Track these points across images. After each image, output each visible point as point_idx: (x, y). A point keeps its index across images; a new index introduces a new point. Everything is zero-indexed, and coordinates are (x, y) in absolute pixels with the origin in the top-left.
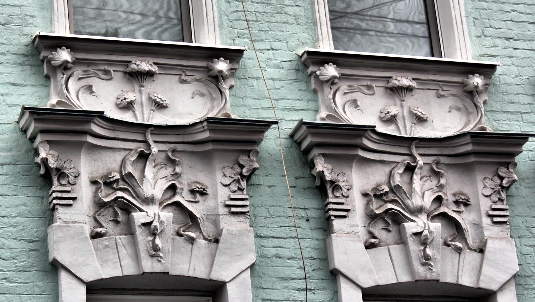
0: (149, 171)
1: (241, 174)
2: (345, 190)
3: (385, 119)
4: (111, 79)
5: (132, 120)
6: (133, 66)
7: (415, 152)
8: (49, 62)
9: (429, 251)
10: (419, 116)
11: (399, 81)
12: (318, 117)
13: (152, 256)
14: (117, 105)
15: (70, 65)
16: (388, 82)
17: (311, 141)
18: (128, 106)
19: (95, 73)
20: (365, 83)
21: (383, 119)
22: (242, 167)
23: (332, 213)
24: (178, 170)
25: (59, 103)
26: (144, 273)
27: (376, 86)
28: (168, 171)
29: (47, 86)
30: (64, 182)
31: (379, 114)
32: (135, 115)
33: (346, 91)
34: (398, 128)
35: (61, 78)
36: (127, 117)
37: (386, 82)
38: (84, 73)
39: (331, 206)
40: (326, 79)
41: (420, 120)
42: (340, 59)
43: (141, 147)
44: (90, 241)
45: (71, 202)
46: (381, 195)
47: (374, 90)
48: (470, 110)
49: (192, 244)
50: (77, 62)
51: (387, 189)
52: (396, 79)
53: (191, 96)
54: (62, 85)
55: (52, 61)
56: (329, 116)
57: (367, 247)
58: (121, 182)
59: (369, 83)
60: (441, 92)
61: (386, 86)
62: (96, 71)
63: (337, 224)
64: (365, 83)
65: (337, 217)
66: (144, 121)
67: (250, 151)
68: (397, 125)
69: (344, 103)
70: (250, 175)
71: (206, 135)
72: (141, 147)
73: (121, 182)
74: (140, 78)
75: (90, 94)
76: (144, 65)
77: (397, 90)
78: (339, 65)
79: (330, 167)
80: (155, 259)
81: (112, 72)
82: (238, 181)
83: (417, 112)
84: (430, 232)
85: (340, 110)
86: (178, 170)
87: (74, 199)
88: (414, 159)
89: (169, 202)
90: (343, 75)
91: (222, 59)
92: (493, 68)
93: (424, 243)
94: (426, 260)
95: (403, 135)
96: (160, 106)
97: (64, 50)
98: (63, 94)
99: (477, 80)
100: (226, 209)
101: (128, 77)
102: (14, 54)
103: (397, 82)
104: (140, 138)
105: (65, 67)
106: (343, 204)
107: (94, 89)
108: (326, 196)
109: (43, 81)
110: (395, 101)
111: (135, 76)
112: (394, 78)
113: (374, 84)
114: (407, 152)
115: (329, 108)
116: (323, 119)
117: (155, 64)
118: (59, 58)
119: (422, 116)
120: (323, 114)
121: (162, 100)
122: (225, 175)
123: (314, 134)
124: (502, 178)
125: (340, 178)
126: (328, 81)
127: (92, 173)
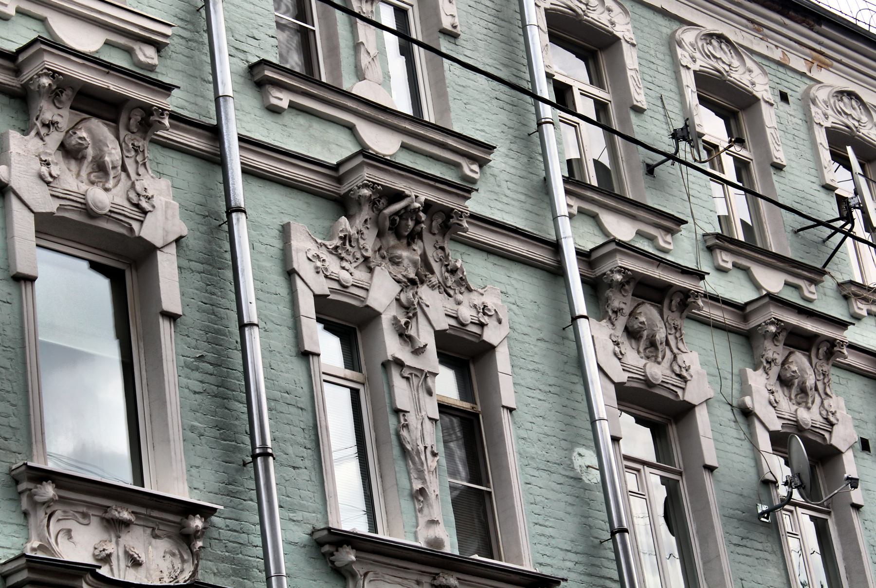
3: (100, 558)
8: (31, 497)
10: (136, 558)
11: (446, 579)
12: (29, 546)
16: (106, 512)
17: (27, 578)
19: (74, 515)
20: (81, 509)
21: (97, 557)
27: (92, 515)
29: (26, 526)
31: (92, 549)
32: (112, 570)
33: (61, 518)
34: (112, 570)
35: (42, 515)
37: (432, 578)
38: (63, 514)
40: (42, 501)
41: (136, 563)
42: (54, 476)
47: (90, 519)
48: (186, 557)
50: (62, 500)
52: (116, 510)
53: (162, 554)
54: (44, 526)
55: (35, 495)
56: (41, 548)
59: (85, 510)
60: (157, 531)
61: (104, 515)
62: (75, 514)
64: (81, 509)
66: (114, 576)
68: (111, 566)
69: (56, 532)
74: (117, 526)
75: (68, 539)
77: (114, 524)
78: (58, 487)
83: (133, 553)
85: (53, 541)
90: (60, 497)
91: (198, 515)
95: (116, 578)
96: (136, 563)
97: (49, 484)
98: (44, 537)
99: (197, 523)
101: (105, 523)
107: (73, 534)
109: (20, 520)
110: (110, 536)
111: (113, 524)
112: (114, 507)
113: (91, 512)
115: (41, 537)
116: (33, 550)
118: (44, 493)
119: (138, 559)
120: (36, 544)
121: (139, 557)
123: (31, 569)
126: (44, 503)
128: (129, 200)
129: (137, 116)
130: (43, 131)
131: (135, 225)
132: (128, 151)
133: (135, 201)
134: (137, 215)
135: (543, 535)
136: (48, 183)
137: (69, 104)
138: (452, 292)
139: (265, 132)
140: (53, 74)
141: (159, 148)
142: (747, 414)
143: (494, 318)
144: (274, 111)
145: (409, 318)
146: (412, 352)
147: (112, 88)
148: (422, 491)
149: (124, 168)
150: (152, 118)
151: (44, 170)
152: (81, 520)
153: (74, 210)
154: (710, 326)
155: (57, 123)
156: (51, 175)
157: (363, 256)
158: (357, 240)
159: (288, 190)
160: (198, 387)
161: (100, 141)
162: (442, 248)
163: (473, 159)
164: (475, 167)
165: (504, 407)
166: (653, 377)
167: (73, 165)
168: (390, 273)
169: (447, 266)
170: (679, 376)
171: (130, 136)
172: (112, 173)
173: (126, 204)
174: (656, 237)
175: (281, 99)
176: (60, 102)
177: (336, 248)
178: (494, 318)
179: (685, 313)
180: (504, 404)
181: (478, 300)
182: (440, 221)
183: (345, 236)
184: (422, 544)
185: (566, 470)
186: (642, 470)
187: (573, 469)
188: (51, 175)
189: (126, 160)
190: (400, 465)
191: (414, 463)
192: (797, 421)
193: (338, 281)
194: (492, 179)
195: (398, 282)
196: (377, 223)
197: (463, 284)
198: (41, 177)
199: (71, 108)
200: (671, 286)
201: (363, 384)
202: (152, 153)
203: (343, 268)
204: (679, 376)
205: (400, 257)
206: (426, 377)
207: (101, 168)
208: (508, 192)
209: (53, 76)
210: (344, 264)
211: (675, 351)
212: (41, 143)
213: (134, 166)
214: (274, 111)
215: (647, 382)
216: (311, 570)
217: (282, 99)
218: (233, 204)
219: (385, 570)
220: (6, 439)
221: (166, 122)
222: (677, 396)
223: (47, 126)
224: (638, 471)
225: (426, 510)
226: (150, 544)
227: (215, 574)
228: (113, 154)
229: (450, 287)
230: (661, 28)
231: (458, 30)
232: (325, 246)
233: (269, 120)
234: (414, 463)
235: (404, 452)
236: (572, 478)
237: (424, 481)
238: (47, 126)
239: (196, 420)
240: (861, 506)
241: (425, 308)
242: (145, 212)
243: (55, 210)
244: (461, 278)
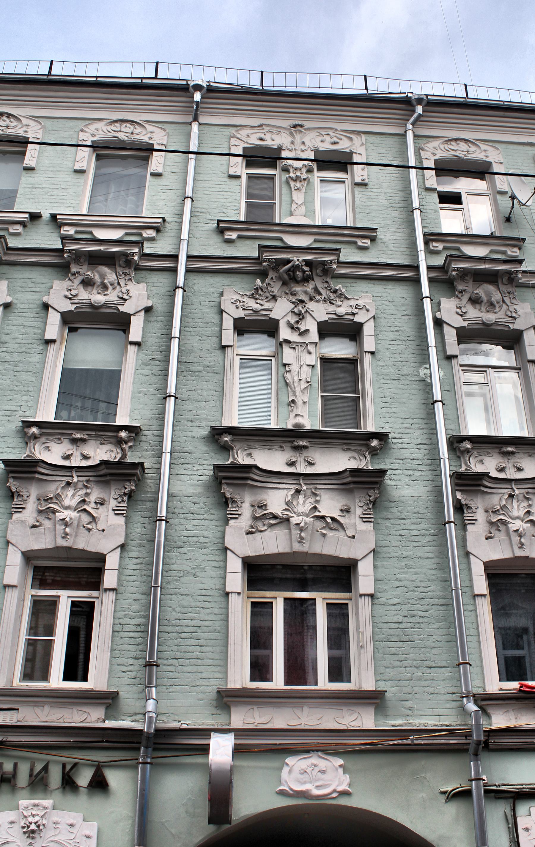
0: (515, 504)
1: (369, 500)
2: (239, 503)
4: (61, 443)
5: (295, 471)
6: (74, 436)
7: (514, 486)
8: (459, 449)
9: (523, 540)
13: (520, 548)
14: (287, 463)
15: (470, 450)
18: (502, 470)
22: (370, 496)
23: (466, 521)
24: (318, 498)
25: (466, 469)
26: (516, 557)
28: (525, 504)
30: (20, 499)
36: (502, 476)
39: (465, 518)
41: (86, 457)
43: (510, 491)
44: (245, 536)
45: (237, 516)
46: (262, 506)
49: (89, 532)
50: (43, 434)
51: (499, 508)
57: (487, 539)
58: (501, 510)
63: (469, 527)
65: (231, 518)
67: (131, 480)
70: (375, 501)
71: (349, 479)
72: (510, 491)
73: (501, 510)
76: (510, 449)
79: (465, 497)
80: (65, 540)
81: (284, 447)
82: (368, 504)
84: (524, 529)
86: (318, 498)
87: (476, 520)
88: (514, 491)
89: (80, 509)
92: (386, 435)
93: (520, 536)
94: (521, 546)
99: (375, 443)
100: (361, 520)
102: (158, 436)
103: (296, 443)
104: (509, 487)
105: (468, 451)
106: (473, 516)
108: (464, 512)
114: (70, 474)
117: (87, 434)
122: (116, 493)
124: (370, 496)
125: (237, 497)
127: (38, 495)
128: (118, 297)
129: (123, 259)
130: (460, 295)
131: (511, 326)
132: (120, 275)
133: (510, 315)
134: (122, 302)
135: (388, 413)
136: (461, 315)
137: (472, 279)
138: (334, 302)
139: (222, 252)
140: (458, 269)
141: (149, 272)
142: (221, 312)
143: (364, 309)
144: (229, 242)
145: (300, 319)
146: (299, 335)
147: (102, 249)
148: (293, 401)
149: (504, 302)
150: (512, 276)
151: (458, 310)
152: (57, 442)
153: (86, 307)
154: (530, 287)
155: (466, 290)
156: (71, 295)
157: (271, 295)
158: (267, 288)
159: (229, 275)
160: (149, 372)
161: (103, 274)
162: (327, 282)
163: (514, 246)
164: (516, 249)
165: (366, 352)
166: (487, 321)
167: (478, 306)
168: (288, 300)
169: (330, 290)
170: (511, 317)
171: (505, 286)
172: (497, 306)
173: (118, 299)
174: (506, 251)
175: (231, 235)
176: (467, 280)
177: (253, 295)
178: (364, 309)
179: (514, 284)
180: (365, 350)
181: (353, 303)
182: (507, 278)
183: (257, 288)
184: (290, 427)
185: (413, 377)
186: (488, 371)
187: (419, 376)
188: (71, 295)
189: (505, 298)
190: (284, 390)
191: (291, 388)
192: (91, 303)
193: (252, 310)
194: (382, 244)
195: (293, 303)
196: (280, 278)
197: (342, 297)
198: (66, 297)
199: (89, 264)
200: (498, 271)
201: (274, 356)
202: (518, 292)
203: (257, 303)
204: (511, 317)
205: (295, 291)
206: (307, 345)
207: (492, 305)
208: (394, 249)
209: (458, 270)
210: (258, 301)
211: (509, 304)
212: (71, 282)
213: (509, 300)
214: (229, 242)
215: (484, 324)
216: (206, 449)
217: (234, 235)
218: (177, 285)
219: (257, 443)
220: (24, 412)
221: (520, 276)
222: (509, 328)
223: (461, 292)
224: (486, 371)
225: (295, 410)
226: (98, 448)
227: (140, 457)
228: (496, 296)
229: (333, 300)
230: (224, 133)
231: (366, 181)
232: (246, 295)
233: (225, 246)
234: (291, 388)
235: (287, 384)
236: (420, 381)
237: (295, 396)
238: (461, 292)
239: (144, 388)
240: (374, 352)
241: (311, 312)
242: (515, 318)
243: (73, 310)
244: (340, 294)
